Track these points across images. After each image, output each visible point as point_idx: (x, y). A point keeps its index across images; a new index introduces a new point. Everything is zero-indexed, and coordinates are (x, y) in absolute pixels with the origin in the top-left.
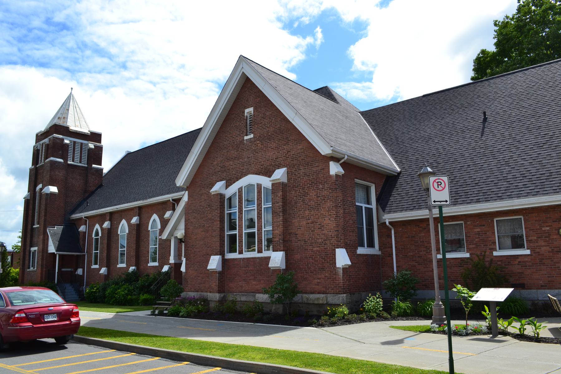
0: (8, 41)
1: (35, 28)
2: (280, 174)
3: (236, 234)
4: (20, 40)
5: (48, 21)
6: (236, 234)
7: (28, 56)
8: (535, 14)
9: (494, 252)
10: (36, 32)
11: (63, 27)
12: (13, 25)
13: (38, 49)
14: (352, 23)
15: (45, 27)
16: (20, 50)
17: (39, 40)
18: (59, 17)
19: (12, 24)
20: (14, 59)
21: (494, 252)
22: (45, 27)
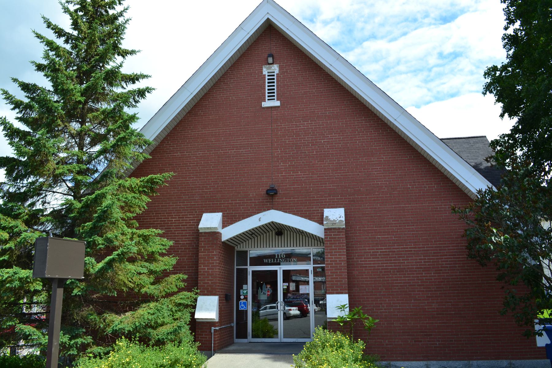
0: (418, 86)
1: (432, 68)
2: (13, 213)
3: (237, 266)
4: (426, 81)
5: (441, 55)
6: (237, 266)
7: (438, 92)
8: (101, 67)
9: (263, 103)
10: (435, 69)
11: (455, 55)
12: (416, 71)
13: (444, 83)
14: (5, 168)
15: (440, 62)
16: (429, 90)
17: (440, 75)
18: (448, 49)
19: (415, 71)
20: (428, 99)
21: (263, 103)
22: (440, 62)
